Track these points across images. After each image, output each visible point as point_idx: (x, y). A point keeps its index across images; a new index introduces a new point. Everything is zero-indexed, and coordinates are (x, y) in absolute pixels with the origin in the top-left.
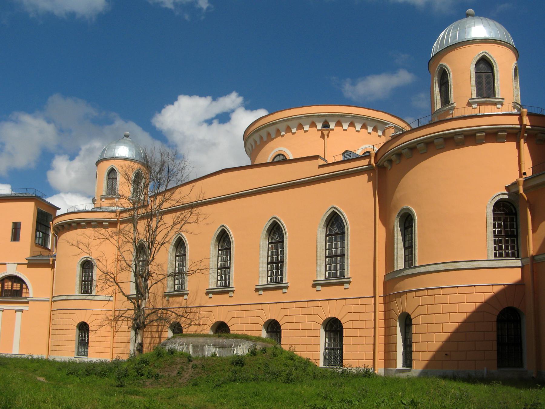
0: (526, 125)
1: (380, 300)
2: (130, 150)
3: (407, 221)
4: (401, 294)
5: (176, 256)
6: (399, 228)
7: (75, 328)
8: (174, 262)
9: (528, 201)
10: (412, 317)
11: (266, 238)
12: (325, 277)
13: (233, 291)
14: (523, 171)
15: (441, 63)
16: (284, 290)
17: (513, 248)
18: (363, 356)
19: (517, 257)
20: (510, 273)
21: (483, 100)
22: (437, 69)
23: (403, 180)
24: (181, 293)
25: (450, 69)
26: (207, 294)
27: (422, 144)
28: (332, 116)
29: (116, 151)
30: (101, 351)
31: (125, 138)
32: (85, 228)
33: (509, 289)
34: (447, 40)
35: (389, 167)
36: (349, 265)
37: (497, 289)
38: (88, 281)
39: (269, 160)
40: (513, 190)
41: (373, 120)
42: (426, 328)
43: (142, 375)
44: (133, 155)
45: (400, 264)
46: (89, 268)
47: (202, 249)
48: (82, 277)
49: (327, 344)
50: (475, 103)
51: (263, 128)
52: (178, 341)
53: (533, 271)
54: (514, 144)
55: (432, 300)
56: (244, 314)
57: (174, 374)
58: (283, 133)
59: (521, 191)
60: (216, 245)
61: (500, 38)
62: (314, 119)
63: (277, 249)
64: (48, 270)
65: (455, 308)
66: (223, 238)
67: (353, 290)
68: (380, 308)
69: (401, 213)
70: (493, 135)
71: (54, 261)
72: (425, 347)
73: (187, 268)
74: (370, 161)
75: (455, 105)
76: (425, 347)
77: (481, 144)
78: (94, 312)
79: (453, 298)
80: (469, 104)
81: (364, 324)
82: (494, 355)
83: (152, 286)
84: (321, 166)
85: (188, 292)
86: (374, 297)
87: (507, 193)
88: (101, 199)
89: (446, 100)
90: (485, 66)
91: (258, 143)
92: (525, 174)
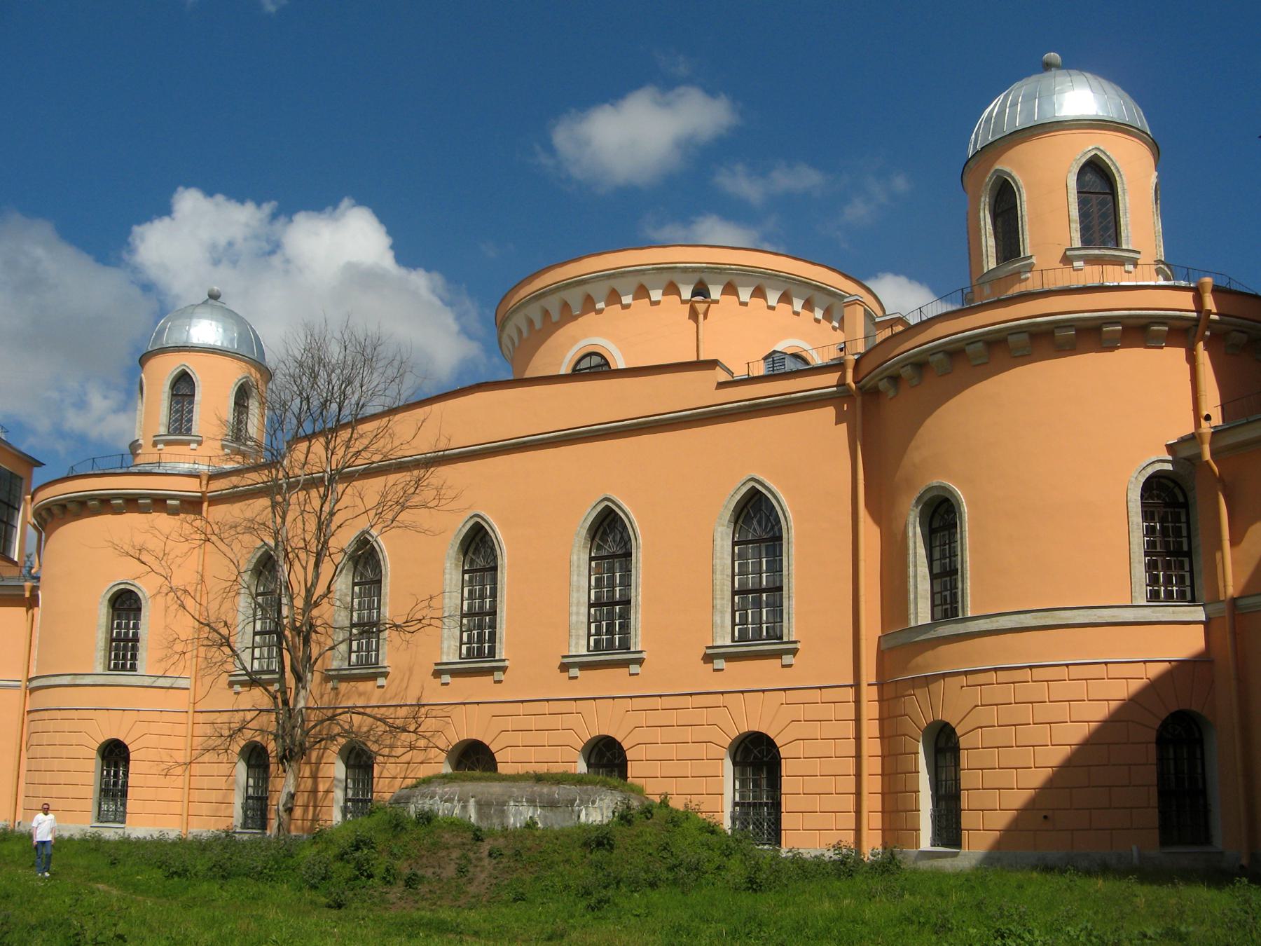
0: (1210, 312)
1: (870, 694)
2: (225, 330)
3: (941, 516)
4: (928, 681)
5: (354, 584)
6: (918, 530)
7: (94, 754)
8: (349, 599)
9: (1221, 479)
10: (959, 731)
11: (585, 547)
12: (733, 640)
13: (504, 669)
14: (1205, 413)
15: (997, 166)
16: (634, 668)
17: (1181, 580)
18: (831, 821)
19: (1193, 601)
20: (1180, 636)
21: (1097, 252)
22: (989, 179)
23: (929, 422)
24: (370, 671)
25: (1020, 180)
26: (437, 674)
27: (980, 344)
28: (716, 270)
29: (192, 331)
30: (156, 815)
31: (212, 301)
32: (122, 513)
33: (1182, 670)
34: (1013, 117)
35: (891, 393)
36: (793, 611)
37: (1155, 671)
38: (127, 640)
39: (565, 369)
40: (1185, 452)
41: (805, 284)
42: (992, 758)
43: (370, 876)
44: (232, 341)
45: (922, 612)
46: (129, 610)
47: (420, 569)
48: (112, 629)
49: (737, 795)
50: (1079, 258)
51: (558, 289)
52: (439, 790)
53: (1235, 633)
54: (1181, 352)
55: (1007, 693)
56: (532, 722)
57: (450, 871)
58: (600, 305)
59: (1207, 456)
60: (457, 559)
61: (1127, 120)
62: (675, 277)
63: (611, 570)
64: (17, 614)
65: (1061, 711)
66: (477, 545)
67: (802, 669)
68: (871, 710)
69: (926, 498)
70: (1140, 331)
71: (34, 589)
72: (993, 799)
73: (387, 613)
74: (843, 377)
75: (1034, 260)
76: (993, 799)
77: (1112, 348)
78: (143, 716)
79: (1059, 691)
80: (1067, 260)
81: (830, 748)
82: (1153, 816)
83: (320, 655)
84: (721, 385)
85: (388, 670)
86: (857, 685)
87: (1170, 458)
88: (155, 444)
89: (1009, 245)
90: (1098, 179)
91: (538, 325)
92: (1208, 418)
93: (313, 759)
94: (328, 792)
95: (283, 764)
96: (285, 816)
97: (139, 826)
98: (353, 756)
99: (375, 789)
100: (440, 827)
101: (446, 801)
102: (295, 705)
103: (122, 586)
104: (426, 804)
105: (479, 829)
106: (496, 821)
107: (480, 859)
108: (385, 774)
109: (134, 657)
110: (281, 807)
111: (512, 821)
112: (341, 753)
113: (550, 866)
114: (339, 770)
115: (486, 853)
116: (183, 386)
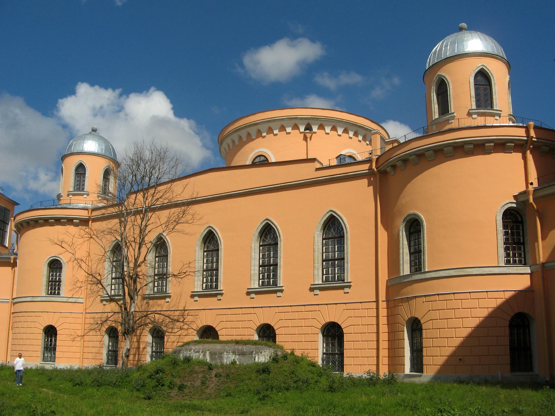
0: (532, 137)
1: (383, 305)
2: (99, 145)
3: (414, 227)
4: (408, 299)
5: (156, 257)
6: (404, 233)
7: (41, 332)
8: (154, 263)
9: (537, 211)
10: (422, 322)
11: (257, 241)
12: (323, 282)
13: (222, 294)
14: (530, 182)
15: (439, 73)
16: (279, 294)
17: (520, 255)
18: (366, 361)
19: (525, 264)
20: (520, 279)
21: (483, 111)
22: (435, 79)
23: (409, 185)
24: (163, 295)
25: (449, 79)
26: (192, 296)
27: (431, 151)
28: (315, 119)
29: (84, 146)
30: (69, 358)
31: (93, 133)
32: (54, 226)
33: (520, 295)
34: (446, 52)
35: (392, 173)
36: (349, 269)
37: (508, 295)
38: (56, 281)
39: (249, 162)
40: (522, 199)
41: (354, 125)
42: (436, 333)
43: (163, 385)
44: (102, 150)
45: (406, 269)
46: (57, 268)
47: (185, 250)
48: (49, 277)
49: (324, 350)
50: (475, 113)
51: (246, 127)
52: (193, 348)
53: (543, 278)
54: (520, 155)
55: (443, 305)
56: (234, 318)
57: (198, 383)
58: (264, 134)
59: (531, 200)
60: (201, 246)
61: (496, 53)
62: (297, 122)
63: (269, 251)
64: (7, 270)
65: (467, 313)
66: (210, 240)
67: (353, 294)
68: (383, 312)
69: (407, 219)
70: (502, 146)
71: (15, 259)
72: (437, 351)
73: (170, 269)
74: (371, 166)
75: (455, 114)
76: (437, 351)
77: (489, 153)
78: (63, 315)
79: (466, 304)
80: (469, 114)
81: (365, 329)
82: (507, 359)
83: (141, 288)
84: (317, 169)
85: (171, 294)
86: (377, 301)
87: (515, 201)
88: (68, 195)
89: (444, 108)
90: (483, 79)
91: (237, 143)
92: (532, 184)
93: (138, 334)
94: (144, 348)
95: (125, 336)
96: (125, 359)
97: (61, 363)
98: (155, 332)
99: (165, 347)
100: (194, 364)
101: (196, 352)
102: (130, 310)
103: (54, 258)
104: (188, 354)
105: (211, 365)
106: (218, 361)
107: (211, 378)
108: (170, 340)
109: (59, 289)
110: (124, 355)
111: (225, 361)
112: (150, 331)
113: (242, 381)
114: (149, 338)
115: (214, 375)
116: (81, 170)
